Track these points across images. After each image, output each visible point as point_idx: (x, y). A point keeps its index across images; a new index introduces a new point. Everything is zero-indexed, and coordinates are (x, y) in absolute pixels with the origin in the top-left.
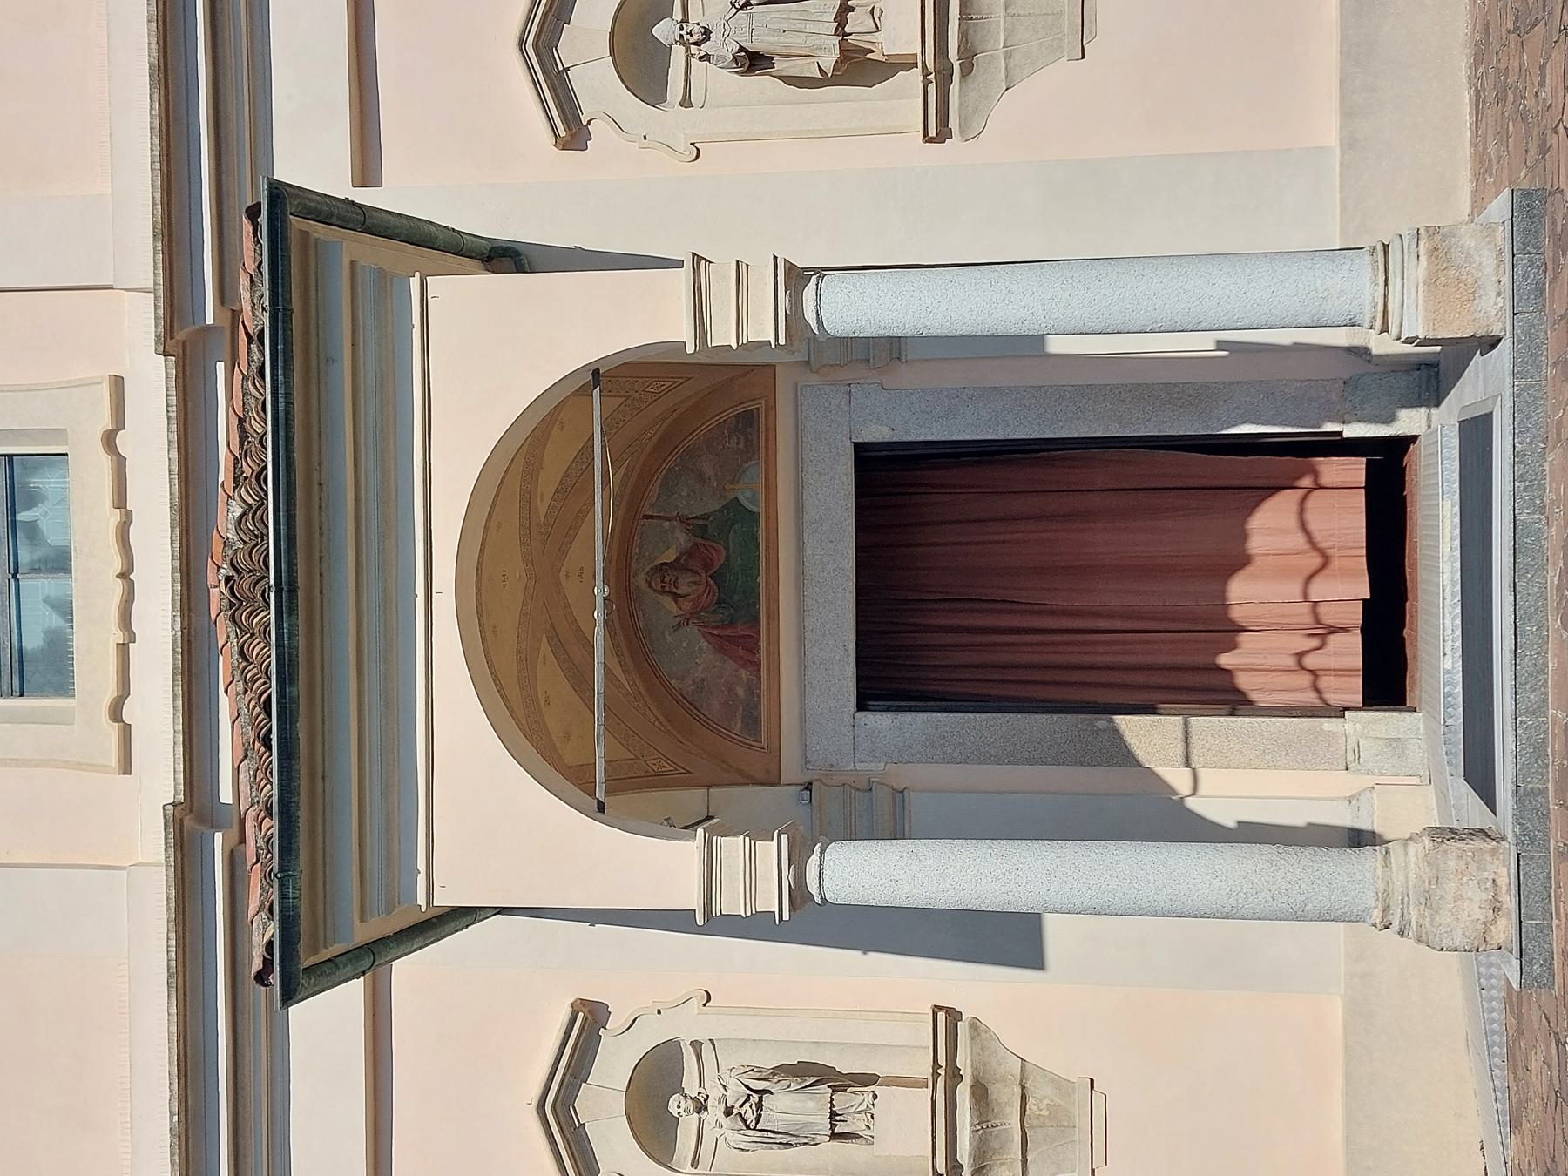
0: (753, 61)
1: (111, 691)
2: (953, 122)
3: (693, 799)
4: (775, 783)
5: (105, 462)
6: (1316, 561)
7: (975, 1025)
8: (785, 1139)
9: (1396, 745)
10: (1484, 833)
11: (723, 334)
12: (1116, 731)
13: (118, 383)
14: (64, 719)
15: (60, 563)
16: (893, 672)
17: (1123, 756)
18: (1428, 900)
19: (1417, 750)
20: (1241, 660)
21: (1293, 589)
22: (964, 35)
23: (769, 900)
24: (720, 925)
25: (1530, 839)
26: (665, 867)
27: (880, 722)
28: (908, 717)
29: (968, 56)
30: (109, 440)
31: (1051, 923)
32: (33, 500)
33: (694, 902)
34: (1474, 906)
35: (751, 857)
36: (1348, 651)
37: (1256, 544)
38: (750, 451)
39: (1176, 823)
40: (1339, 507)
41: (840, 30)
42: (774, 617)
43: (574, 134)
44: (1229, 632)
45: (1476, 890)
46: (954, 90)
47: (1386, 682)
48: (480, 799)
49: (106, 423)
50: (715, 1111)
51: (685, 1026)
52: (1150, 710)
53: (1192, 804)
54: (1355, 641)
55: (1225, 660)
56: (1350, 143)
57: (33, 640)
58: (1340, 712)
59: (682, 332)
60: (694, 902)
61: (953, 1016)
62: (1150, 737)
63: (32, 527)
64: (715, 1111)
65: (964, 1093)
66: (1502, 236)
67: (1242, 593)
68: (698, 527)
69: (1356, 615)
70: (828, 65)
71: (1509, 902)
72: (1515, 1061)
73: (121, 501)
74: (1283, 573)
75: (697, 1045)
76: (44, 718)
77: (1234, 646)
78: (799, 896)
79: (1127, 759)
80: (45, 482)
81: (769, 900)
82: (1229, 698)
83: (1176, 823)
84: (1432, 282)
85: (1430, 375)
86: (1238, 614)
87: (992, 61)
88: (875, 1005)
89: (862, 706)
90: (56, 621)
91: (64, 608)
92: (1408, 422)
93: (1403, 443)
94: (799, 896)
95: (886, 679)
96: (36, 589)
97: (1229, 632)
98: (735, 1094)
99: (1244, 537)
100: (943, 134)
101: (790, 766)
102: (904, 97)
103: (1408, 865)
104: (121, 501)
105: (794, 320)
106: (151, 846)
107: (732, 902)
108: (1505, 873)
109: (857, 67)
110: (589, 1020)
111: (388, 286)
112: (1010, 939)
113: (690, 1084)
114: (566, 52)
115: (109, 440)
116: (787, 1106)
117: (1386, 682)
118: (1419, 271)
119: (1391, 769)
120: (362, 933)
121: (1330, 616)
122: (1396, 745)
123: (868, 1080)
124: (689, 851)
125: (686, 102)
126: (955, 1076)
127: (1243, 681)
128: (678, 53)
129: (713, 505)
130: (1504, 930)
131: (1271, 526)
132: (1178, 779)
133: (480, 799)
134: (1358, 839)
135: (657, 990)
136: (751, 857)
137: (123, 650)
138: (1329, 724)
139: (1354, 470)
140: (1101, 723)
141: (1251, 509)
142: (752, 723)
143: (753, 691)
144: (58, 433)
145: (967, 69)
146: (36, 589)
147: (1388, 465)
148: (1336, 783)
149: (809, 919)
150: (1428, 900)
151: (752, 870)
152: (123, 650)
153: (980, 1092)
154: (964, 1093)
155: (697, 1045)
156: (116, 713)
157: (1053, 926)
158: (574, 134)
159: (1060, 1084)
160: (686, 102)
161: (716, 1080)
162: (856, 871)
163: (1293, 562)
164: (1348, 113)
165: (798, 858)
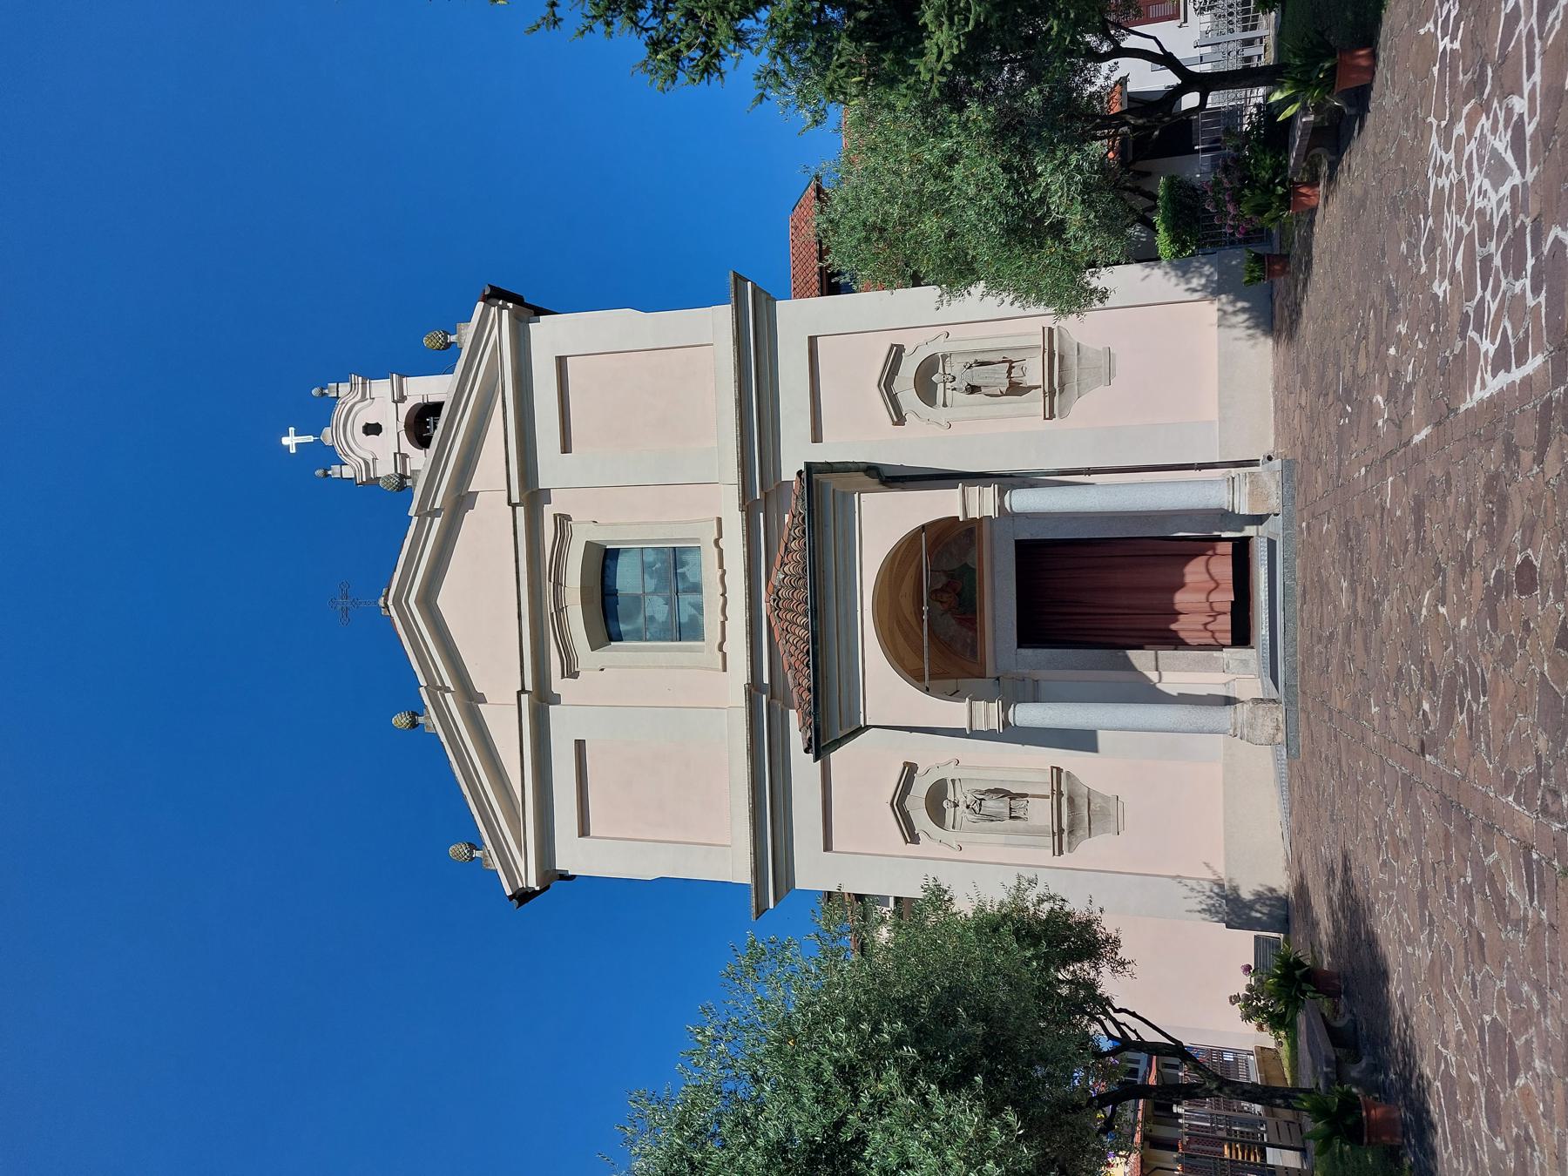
0: (973, 389)
1: (719, 640)
2: (1056, 412)
3: (951, 684)
4: (983, 676)
5: (716, 550)
6: (1213, 585)
7: (1068, 773)
8: (991, 818)
9: (1245, 663)
10: (1274, 701)
11: (974, 513)
12: (1127, 657)
13: (719, 520)
14: (701, 650)
15: (697, 589)
16: (1032, 633)
17: (1130, 667)
18: (1251, 726)
19: (1253, 664)
20: (1180, 626)
21: (1203, 597)
22: (1060, 377)
23: (994, 724)
24: (975, 735)
25: (1290, 703)
26: (954, 713)
27: (1023, 651)
28: (1039, 651)
29: (1062, 385)
30: (716, 542)
31: (1100, 733)
32: (683, 565)
33: (966, 725)
34: (1269, 729)
35: (987, 710)
36: (1225, 622)
37: (1188, 579)
38: (972, 543)
39: (1155, 696)
40: (1223, 568)
41: (1009, 376)
42: (982, 610)
43: (900, 420)
44: (1175, 614)
45: (1270, 722)
46: (1056, 399)
47: (1241, 636)
48: (883, 687)
49: (716, 536)
50: (962, 807)
51: (948, 774)
52: (1140, 647)
53: (1159, 686)
54: (1229, 617)
55: (1173, 627)
56: (1223, 420)
57: (684, 619)
58: (1222, 647)
59: (959, 513)
60: (966, 725)
61: (1059, 770)
62: (1141, 659)
63: (683, 574)
64: (962, 807)
65: (1064, 800)
66: (1278, 476)
67: (1181, 599)
68: (950, 575)
69: (1228, 608)
70: (1004, 390)
71: (1283, 727)
72: (1290, 788)
73: (721, 566)
74: (1198, 590)
75: (953, 781)
76: (691, 650)
77: (1176, 621)
78: (1006, 723)
79: (1132, 668)
80: (689, 558)
81: (994, 724)
82: (1175, 642)
83: (1155, 696)
84: (1251, 494)
85: (1259, 520)
86: (1178, 607)
87: (1073, 385)
88: (1028, 766)
89: (1019, 646)
90: (694, 612)
91: (699, 608)
92: (1250, 531)
93: (1249, 538)
94: (1006, 723)
95: (1032, 633)
96: (686, 599)
97: (1175, 614)
98: (970, 798)
99: (1183, 575)
100: (1052, 416)
101: (990, 671)
102: (1035, 403)
103: (1243, 712)
104: (721, 566)
105: (1001, 507)
106: (740, 699)
107: (980, 725)
108: (1281, 717)
109: (1015, 389)
110: (910, 770)
111: (847, 499)
112: (1084, 740)
113: (950, 796)
114: (896, 387)
115: (716, 542)
116: (991, 805)
117: (1241, 636)
118: (1246, 489)
119: (1238, 673)
120: (841, 734)
121: (1217, 607)
122: (1245, 663)
123: (1025, 796)
124: (963, 706)
125: (945, 405)
126: (1060, 794)
127: (1182, 635)
128: (940, 387)
129: (955, 565)
130: (1281, 737)
131: (1194, 571)
132: (1153, 676)
133: (883, 687)
134: (1229, 701)
135: (935, 758)
136: (987, 710)
137: (723, 624)
138: (1216, 654)
139: (1227, 548)
140: (1120, 653)
141: (1185, 564)
142: (974, 653)
143: (974, 641)
144: (697, 540)
145: (1062, 391)
146: (686, 599)
147: (1242, 549)
148: (1221, 678)
149: (1011, 734)
150: (1251, 726)
151: (988, 714)
152: (723, 624)
153: (1071, 800)
154: (1064, 800)
155: (953, 781)
156: (720, 649)
157: (1102, 736)
158: (900, 420)
159: (1104, 797)
160: (945, 405)
161: (962, 794)
162: (1028, 714)
163: (1201, 590)
164: (1221, 407)
165: (1005, 710)
